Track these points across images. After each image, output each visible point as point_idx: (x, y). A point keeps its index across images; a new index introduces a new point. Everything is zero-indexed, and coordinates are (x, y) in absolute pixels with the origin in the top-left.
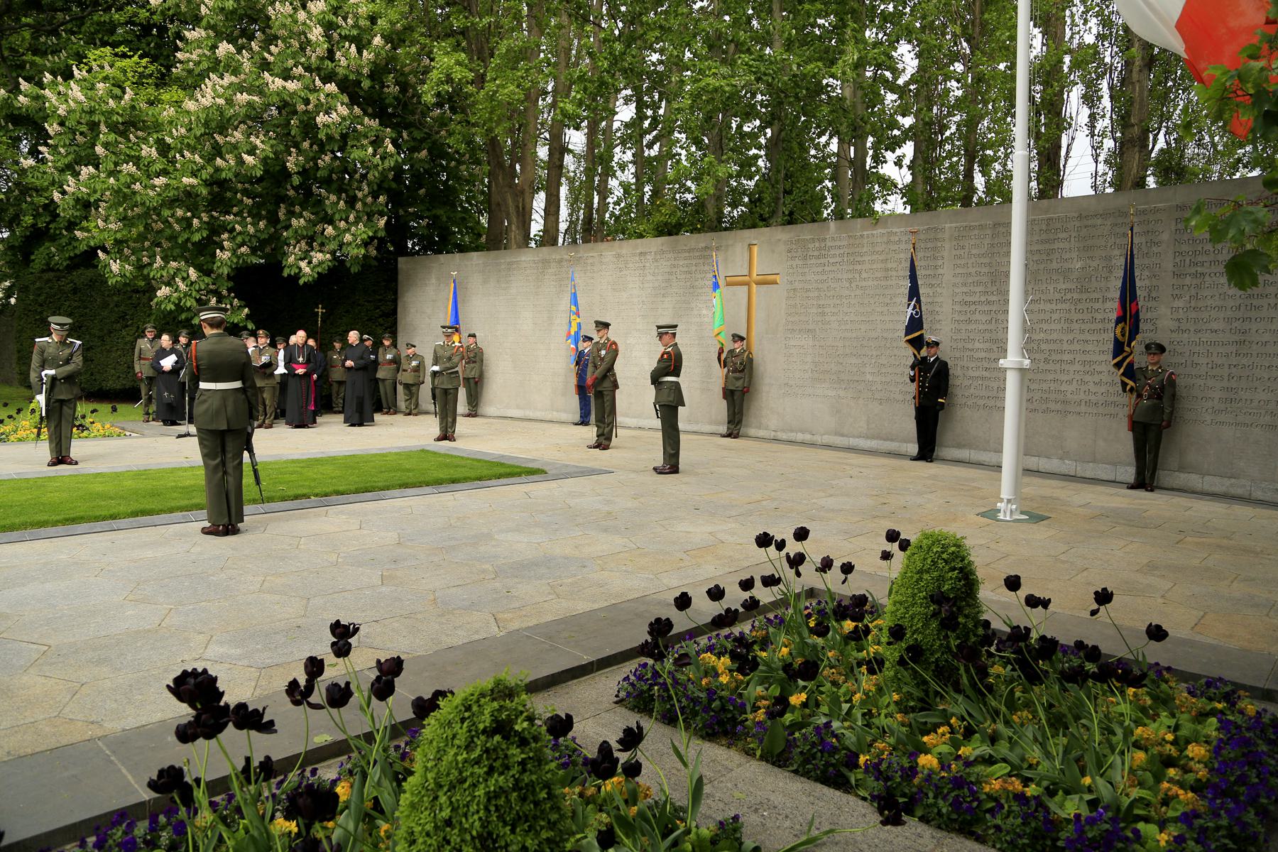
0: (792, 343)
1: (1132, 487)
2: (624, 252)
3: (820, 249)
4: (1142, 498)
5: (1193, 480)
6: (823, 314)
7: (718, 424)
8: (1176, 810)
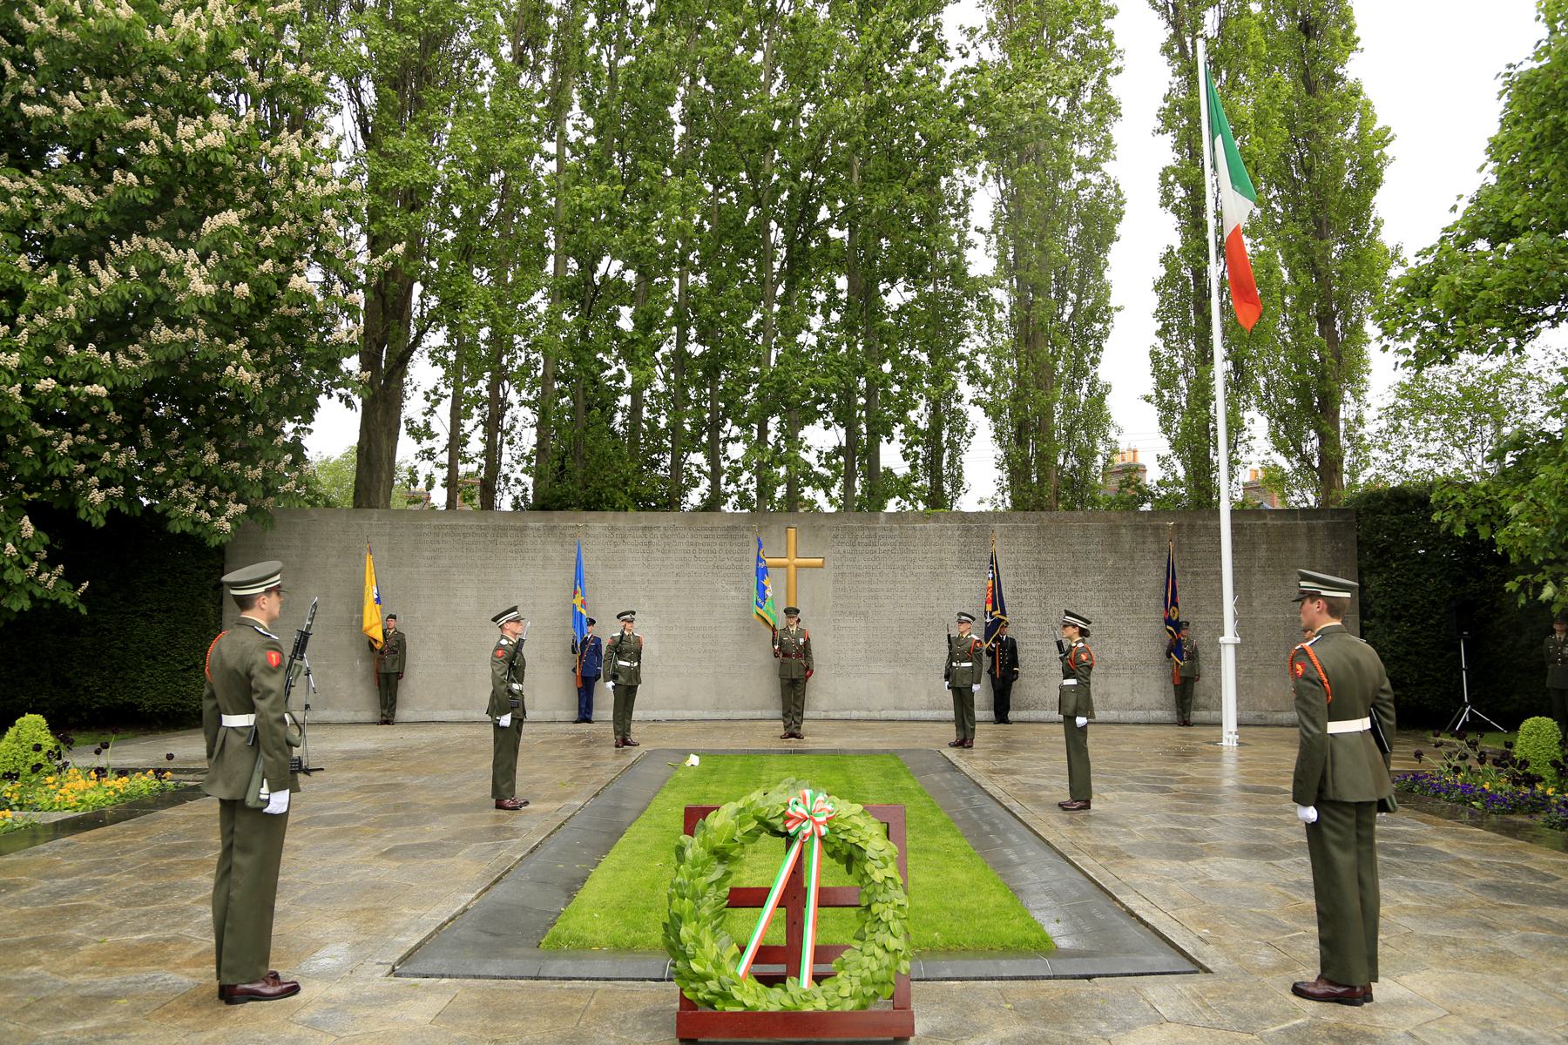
4: (584, 727)
5: (1023, 715)
6: (876, 598)
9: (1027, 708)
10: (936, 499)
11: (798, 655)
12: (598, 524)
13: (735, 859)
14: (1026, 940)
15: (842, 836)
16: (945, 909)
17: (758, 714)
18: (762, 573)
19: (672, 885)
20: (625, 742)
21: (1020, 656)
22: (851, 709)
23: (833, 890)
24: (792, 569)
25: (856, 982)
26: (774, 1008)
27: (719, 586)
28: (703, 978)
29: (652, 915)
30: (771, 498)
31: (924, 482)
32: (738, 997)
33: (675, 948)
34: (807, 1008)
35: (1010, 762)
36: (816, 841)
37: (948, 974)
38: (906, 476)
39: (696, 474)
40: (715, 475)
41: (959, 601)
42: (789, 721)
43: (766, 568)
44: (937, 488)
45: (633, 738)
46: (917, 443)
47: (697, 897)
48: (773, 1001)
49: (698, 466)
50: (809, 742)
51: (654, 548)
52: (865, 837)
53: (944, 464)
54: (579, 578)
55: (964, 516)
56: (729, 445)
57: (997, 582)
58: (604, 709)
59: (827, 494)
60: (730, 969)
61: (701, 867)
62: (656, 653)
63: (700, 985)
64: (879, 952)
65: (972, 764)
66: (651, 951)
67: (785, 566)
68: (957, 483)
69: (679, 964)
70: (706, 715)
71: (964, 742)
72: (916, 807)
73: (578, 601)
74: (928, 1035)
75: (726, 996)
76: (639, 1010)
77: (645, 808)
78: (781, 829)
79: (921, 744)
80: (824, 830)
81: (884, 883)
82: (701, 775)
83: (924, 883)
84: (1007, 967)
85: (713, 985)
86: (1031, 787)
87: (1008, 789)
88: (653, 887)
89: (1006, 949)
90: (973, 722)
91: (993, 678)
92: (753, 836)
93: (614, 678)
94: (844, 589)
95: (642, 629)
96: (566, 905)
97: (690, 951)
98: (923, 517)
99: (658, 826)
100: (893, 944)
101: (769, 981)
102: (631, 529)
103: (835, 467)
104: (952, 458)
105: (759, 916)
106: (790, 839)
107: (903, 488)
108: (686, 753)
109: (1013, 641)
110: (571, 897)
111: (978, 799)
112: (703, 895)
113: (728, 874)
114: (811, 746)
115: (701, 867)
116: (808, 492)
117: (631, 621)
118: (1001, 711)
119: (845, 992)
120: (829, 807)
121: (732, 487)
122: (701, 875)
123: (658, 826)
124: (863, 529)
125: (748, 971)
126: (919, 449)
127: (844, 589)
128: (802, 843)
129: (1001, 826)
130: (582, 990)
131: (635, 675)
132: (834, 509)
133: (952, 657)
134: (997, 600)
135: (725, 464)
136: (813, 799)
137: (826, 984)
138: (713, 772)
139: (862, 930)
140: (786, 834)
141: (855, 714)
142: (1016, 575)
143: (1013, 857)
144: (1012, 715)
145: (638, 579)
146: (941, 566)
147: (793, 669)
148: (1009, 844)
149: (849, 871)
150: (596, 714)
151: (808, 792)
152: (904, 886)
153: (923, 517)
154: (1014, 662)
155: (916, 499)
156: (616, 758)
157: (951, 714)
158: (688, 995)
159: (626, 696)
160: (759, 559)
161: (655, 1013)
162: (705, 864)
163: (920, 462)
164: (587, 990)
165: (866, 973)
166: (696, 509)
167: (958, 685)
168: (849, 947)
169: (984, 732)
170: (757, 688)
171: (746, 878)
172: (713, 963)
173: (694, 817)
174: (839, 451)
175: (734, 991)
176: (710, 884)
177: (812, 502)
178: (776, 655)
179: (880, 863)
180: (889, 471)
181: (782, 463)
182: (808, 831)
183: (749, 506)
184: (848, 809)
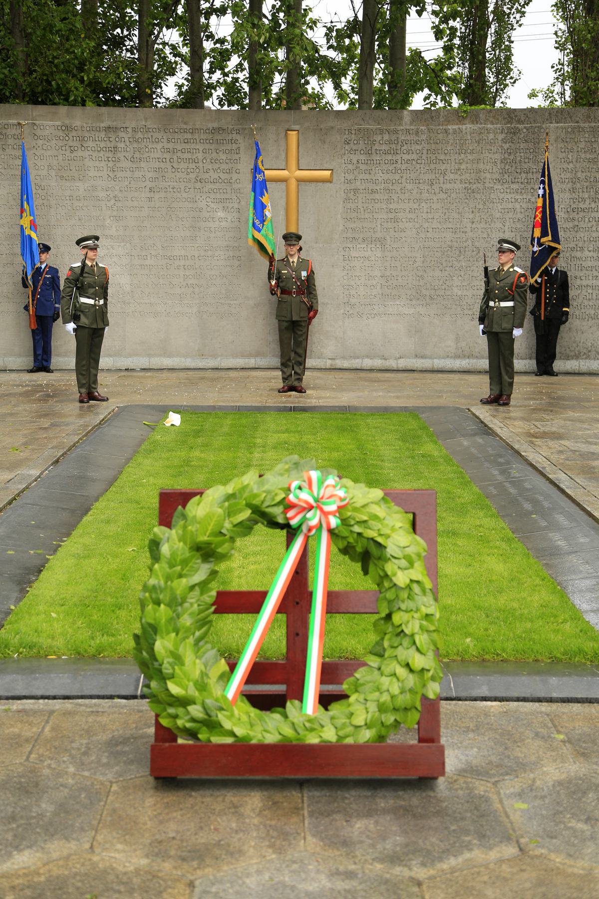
0: (354, 254)
1: (31, 371)
2: (77, 123)
3: (390, 142)
4: (41, 378)
5: (572, 365)
6: (396, 220)
7: (257, 354)
8: (209, 597)
9: (577, 357)
10: (476, 93)
11: (300, 292)
12: (48, 121)
13: (223, 557)
14: (580, 651)
15: (357, 529)
16: (479, 608)
17: (252, 362)
18: (259, 187)
19: (145, 588)
20: (91, 396)
21: (572, 293)
22: (363, 357)
24: (293, 184)
25: (373, 707)
26: (271, 738)
27: (202, 204)
28: (184, 702)
29: (123, 613)
30: (268, 92)
31: (460, 70)
32: (227, 725)
33: (150, 666)
34: (313, 739)
35: (555, 424)
36: (325, 535)
37: (484, 691)
38: (438, 61)
39: (171, 58)
40: (195, 59)
41: (499, 225)
42: (288, 371)
43: (264, 181)
44: (477, 76)
45: (101, 391)
46: (454, 15)
47: (175, 603)
48: (269, 729)
49: (173, 47)
50: (312, 397)
51: (120, 155)
53: (489, 44)
54: (25, 192)
55: (511, 115)
56: (213, 19)
57: (549, 198)
58: (66, 355)
59: (337, 86)
60: (217, 691)
61: (179, 567)
62: (128, 288)
63: (180, 711)
64: (401, 672)
65: (508, 425)
66: (122, 659)
67: (284, 180)
68: (504, 68)
69: (153, 684)
70: (189, 363)
71: (499, 398)
72: (439, 478)
73: (26, 222)
74: (462, 772)
75: (212, 725)
76: (104, 737)
77: (115, 479)
78: (281, 520)
79: (446, 400)
80: (334, 522)
81: (409, 587)
82: (184, 437)
83: (457, 579)
84: (557, 685)
85: (196, 711)
86: (583, 455)
87: (554, 458)
88: (124, 578)
89: (555, 661)
90: (511, 373)
91: (537, 319)
92: (245, 528)
93: (75, 318)
94: (356, 210)
95: (108, 258)
96: (19, 600)
97: (167, 669)
98: (458, 116)
99: (129, 501)
100: (418, 661)
101: (264, 703)
102: (92, 129)
103: (348, 50)
104: (499, 35)
105: (253, 623)
106: (291, 532)
107: (434, 77)
108: (164, 410)
109: (564, 274)
110: (23, 592)
111: (517, 470)
112: (184, 600)
113: (214, 573)
114: (313, 402)
115: (179, 567)
116: (313, 84)
117: (94, 249)
118: (545, 362)
119: (359, 720)
120: (341, 493)
121: (217, 75)
122: (180, 576)
123: (129, 501)
124: (381, 132)
126: (456, 24)
127: (356, 210)
128: (307, 538)
129: (546, 504)
130: (35, 712)
131: (101, 316)
132: (344, 107)
133: (489, 295)
134: (548, 222)
135: (208, 45)
136: (322, 482)
137: (336, 709)
138: (197, 433)
139: (380, 643)
140: (286, 526)
141: (368, 363)
142: (573, 190)
143: (561, 543)
144: (558, 365)
145: (102, 194)
146: (478, 180)
147: (293, 308)
148: (558, 528)
149: (366, 571)
150: (56, 361)
151: (315, 475)
153: (458, 116)
154: (565, 300)
155: (449, 93)
156: (80, 416)
157: (484, 364)
158: (164, 722)
159: (90, 341)
160: (256, 170)
161: (125, 741)
162: (185, 562)
163: (457, 41)
164: (41, 712)
165: (385, 698)
166: (173, 105)
167: (496, 329)
169: (524, 387)
170: (247, 333)
171: (239, 575)
172: (196, 683)
173: (171, 504)
174: (353, 26)
175: (221, 717)
176: (192, 588)
177: (318, 97)
178: (273, 292)
179: (404, 563)
180: (417, 54)
181: (281, 44)
182: (314, 522)
183: (239, 102)
184: (365, 496)
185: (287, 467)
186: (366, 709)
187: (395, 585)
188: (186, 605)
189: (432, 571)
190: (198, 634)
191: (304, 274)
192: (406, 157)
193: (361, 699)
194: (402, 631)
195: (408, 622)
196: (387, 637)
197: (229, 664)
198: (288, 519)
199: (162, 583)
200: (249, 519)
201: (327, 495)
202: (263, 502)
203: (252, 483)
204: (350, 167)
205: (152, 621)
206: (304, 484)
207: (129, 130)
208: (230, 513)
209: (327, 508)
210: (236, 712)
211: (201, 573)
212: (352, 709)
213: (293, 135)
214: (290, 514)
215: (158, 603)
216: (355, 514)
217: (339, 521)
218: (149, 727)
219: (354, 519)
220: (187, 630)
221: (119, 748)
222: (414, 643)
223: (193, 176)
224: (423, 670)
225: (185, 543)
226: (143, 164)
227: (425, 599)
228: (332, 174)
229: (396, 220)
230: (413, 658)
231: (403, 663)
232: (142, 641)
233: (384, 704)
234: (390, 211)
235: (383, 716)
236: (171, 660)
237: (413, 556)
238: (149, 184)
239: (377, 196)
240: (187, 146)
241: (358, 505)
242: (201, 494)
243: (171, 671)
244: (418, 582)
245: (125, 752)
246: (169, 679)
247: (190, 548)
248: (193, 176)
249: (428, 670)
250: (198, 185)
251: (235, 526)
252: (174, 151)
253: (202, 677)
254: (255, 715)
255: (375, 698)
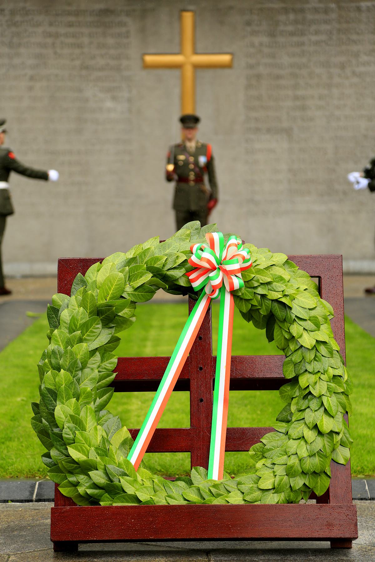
15: (260, 291)
23: (251, 360)
24: (189, 71)
25: (280, 470)
28: (85, 468)
32: (130, 490)
34: (217, 502)
36: (228, 298)
47: (77, 367)
52: (288, 292)
63: (81, 478)
64: (310, 435)
69: (54, 453)
75: (113, 489)
78: (182, 283)
80: (238, 282)
85: (98, 477)
97: (67, 434)
99: (17, 366)
100: (327, 424)
106: (192, 295)
112: (84, 366)
113: (115, 340)
119: (267, 484)
120: (244, 253)
122: (81, 340)
123: (17, 366)
124: (286, 11)
125: (140, 460)
136: (224, 245)
149: (270, 337)
152: (342, 353)
158: (64, 491)
162: (85, 327)
165: (293, 461)
168: (271, 430)
171: (138, 344)
175: (124, 483)
176: (93, 353)
178: (169, 178)
179: (309, 325)
182: (217, 281)
185: (188, 232)
186: (274, 472)
187: (302, 346)
188: (86, 370)
189: (340, 335)
190: (99, 401)
191: (203, 160)
192: (314, 38)
193: (268, 463)
194: (310, 393)
195: (316, 383)
196: (294, 401)
197: (130, 431)
198: (190, 281)
199: (62, 348)
200: (150, 283)
201: (229, 256)
202: (164, 266)
203: (153, 248)
204: (252, 50)
205: (52, 387)
206: (204, 245)
207: (7, 12)
208: (130, 278)
209: (228, 268)
210: (139, 478)
211: (103, 337)
212: (258, 474)
213: (188, 17)
214: (192, 277)
215: (58, 368)
216: (259, 276)
217: (242, 282)
218: (47, 519)
219: (258, 281)
220: (88, 395)
221: (15, 533)
222: (322, 404)
223: (77, 63)
224: (332, 432)
225: (85, 308)
226: (22, 50)
227: (332, 361)
228: (232, 60)
229: (304, 108)
230: (322, 421)
231: (311, 426)
232: (42, 408)
233: (292, 467)
234: (296, 98)
235: (291, 480)
236: (71, 425)
237: (320, 319)
238: (30, 72)
239: (283, 82)
240: (71, 30)
241: (261, 267)
242: (101, 260)
243: (72, 436)
244: (324, 343)
245: (22, 536)
246: (69, 444)
247: (90, 313)
248: (77, 63)
249: (338, 433)
250: (84, 72)
251: (136, 289)
252: (57, 35)
253: (104, 443)
254: (159, 481)
255: (283, 462)
